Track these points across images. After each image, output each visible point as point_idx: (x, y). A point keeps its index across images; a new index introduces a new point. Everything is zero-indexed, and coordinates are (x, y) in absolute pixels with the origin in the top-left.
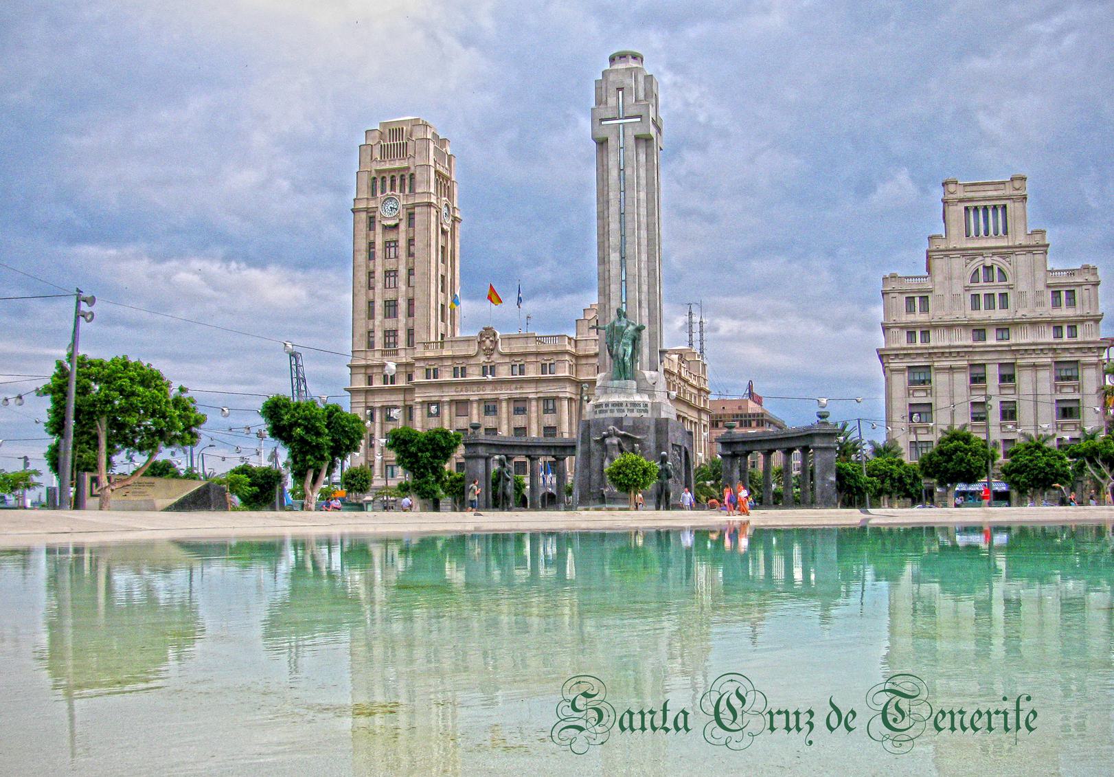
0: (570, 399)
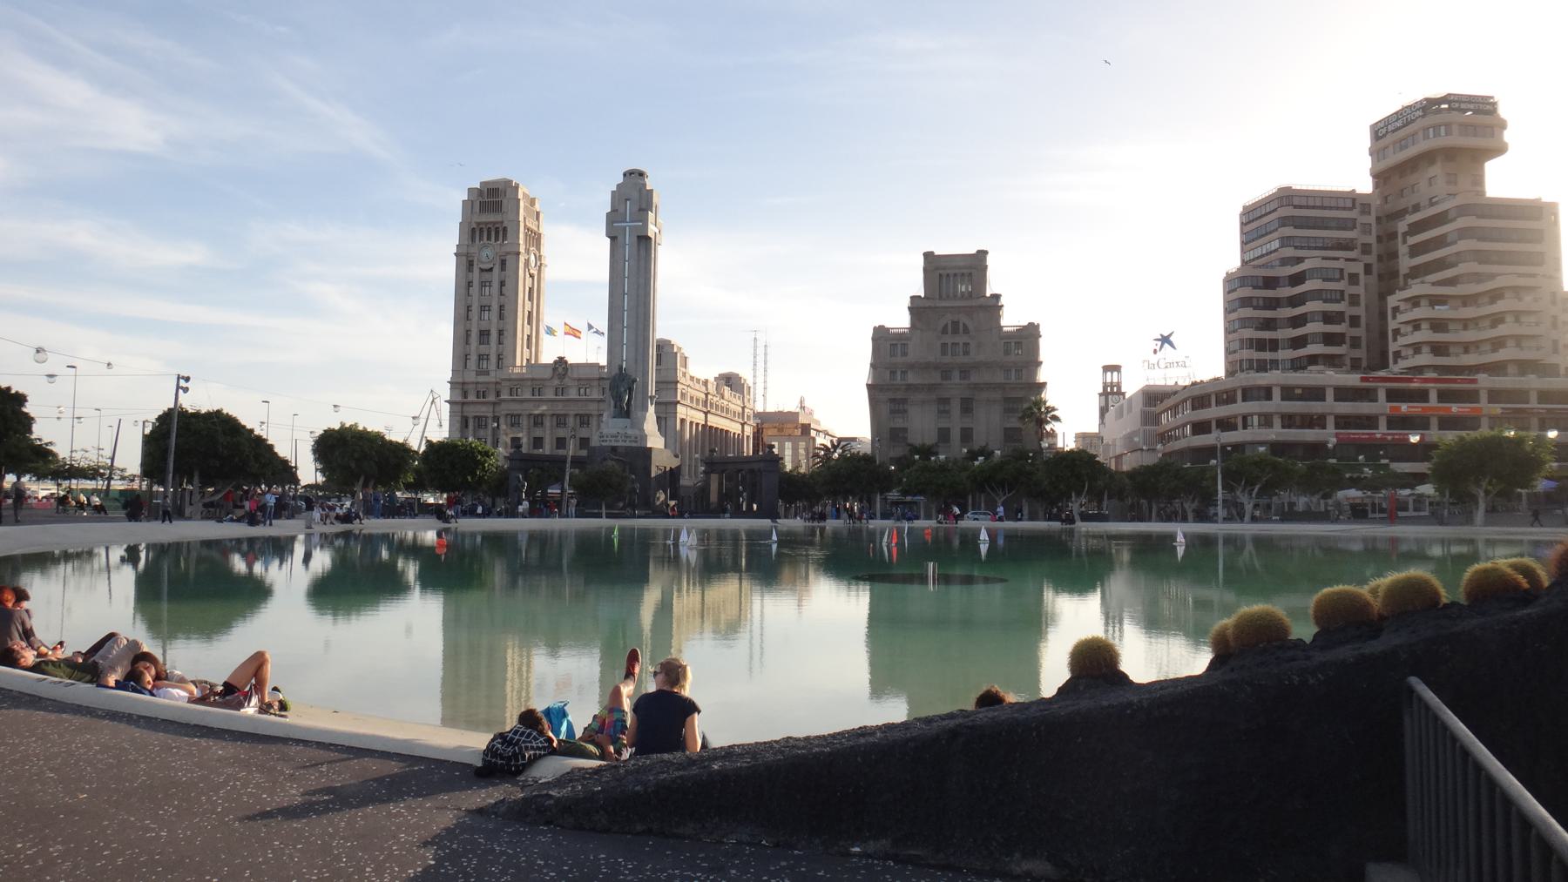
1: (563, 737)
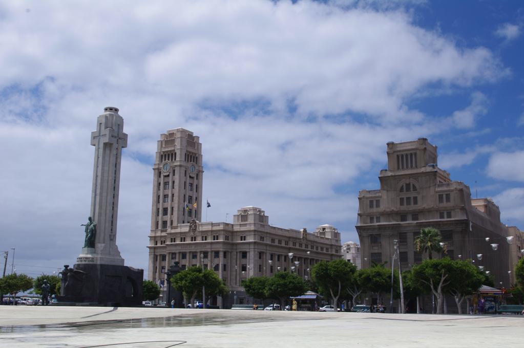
0: (180, 166)
1: (463, 298)
